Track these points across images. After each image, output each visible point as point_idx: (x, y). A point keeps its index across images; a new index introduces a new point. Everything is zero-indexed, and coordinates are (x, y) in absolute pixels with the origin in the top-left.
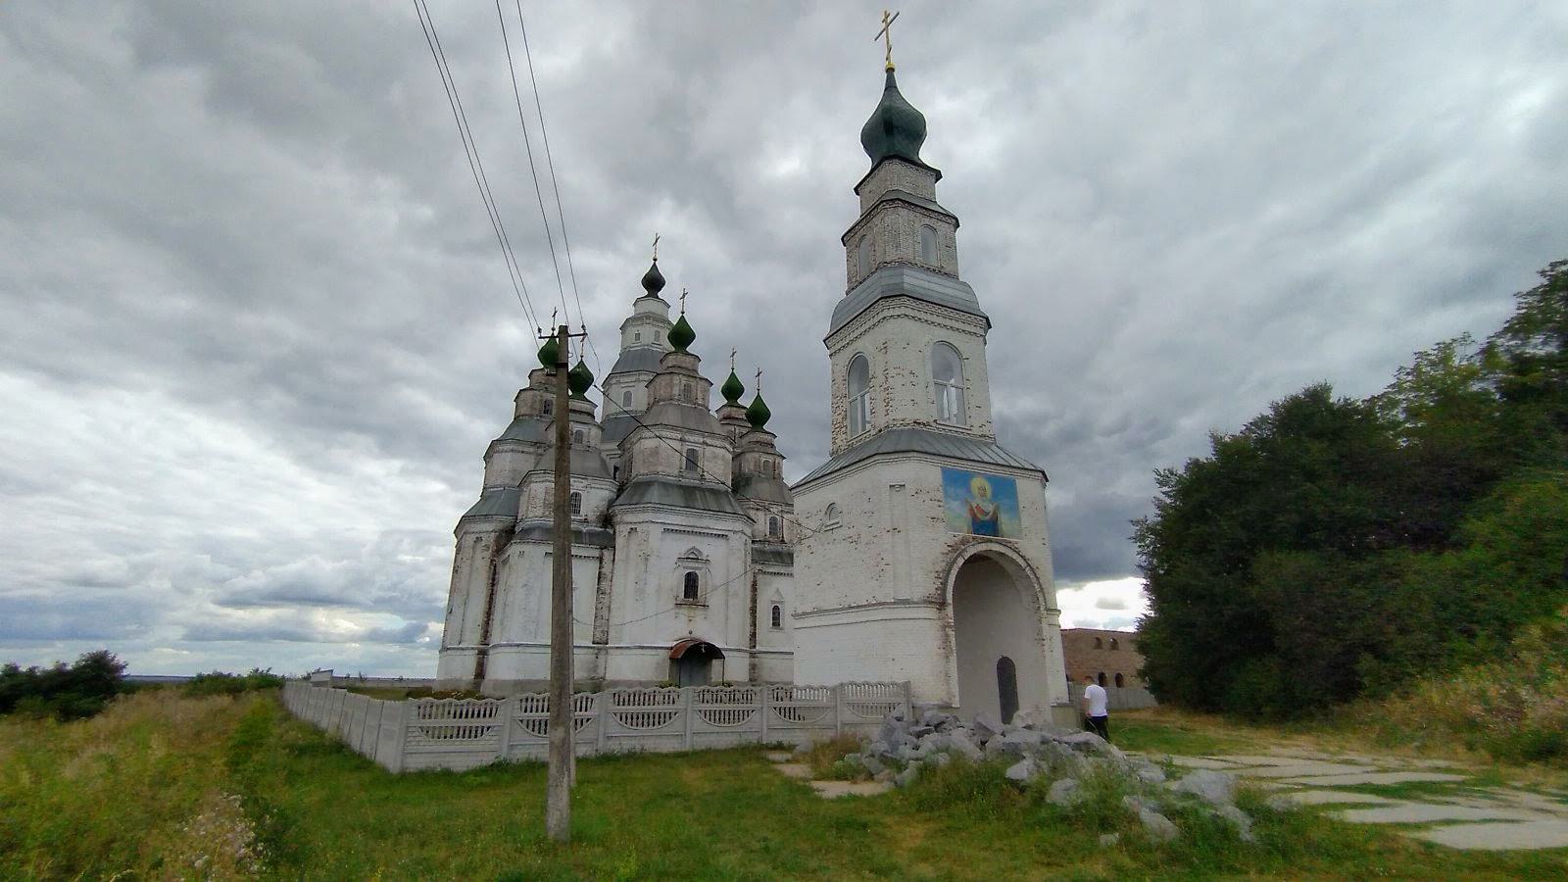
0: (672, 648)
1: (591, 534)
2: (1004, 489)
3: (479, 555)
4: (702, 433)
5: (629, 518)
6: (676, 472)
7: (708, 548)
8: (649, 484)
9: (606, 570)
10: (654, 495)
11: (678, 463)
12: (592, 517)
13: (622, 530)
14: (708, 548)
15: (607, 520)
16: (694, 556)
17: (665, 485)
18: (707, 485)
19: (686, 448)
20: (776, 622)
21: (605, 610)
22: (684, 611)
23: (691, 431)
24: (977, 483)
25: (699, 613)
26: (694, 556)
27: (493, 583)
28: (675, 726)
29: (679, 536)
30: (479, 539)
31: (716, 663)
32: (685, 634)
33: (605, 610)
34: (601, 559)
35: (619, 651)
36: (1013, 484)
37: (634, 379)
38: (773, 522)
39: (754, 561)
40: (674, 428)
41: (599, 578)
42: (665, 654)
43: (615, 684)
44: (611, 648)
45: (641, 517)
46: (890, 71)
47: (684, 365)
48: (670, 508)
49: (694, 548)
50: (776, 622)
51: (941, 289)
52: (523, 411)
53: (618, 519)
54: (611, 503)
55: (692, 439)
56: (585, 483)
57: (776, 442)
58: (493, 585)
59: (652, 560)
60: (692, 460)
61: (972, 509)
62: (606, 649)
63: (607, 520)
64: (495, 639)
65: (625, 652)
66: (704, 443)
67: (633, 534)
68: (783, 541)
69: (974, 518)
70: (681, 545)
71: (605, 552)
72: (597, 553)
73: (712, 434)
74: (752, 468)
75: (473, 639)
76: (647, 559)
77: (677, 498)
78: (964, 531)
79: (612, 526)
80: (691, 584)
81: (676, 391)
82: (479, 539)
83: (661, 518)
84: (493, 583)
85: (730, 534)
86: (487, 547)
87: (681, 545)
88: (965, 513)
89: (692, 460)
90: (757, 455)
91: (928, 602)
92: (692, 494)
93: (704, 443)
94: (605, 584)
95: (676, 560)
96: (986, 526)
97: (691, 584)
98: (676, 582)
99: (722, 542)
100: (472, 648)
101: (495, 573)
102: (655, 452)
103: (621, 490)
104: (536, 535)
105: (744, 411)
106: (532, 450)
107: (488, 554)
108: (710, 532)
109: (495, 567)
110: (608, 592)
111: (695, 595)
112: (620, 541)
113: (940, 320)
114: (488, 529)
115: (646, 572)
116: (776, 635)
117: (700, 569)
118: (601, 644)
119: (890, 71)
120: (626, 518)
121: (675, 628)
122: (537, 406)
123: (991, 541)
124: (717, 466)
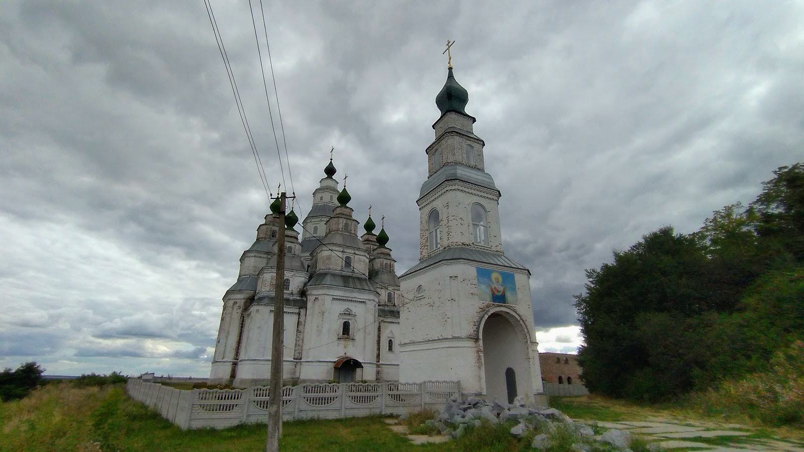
0: (335, 362)
1: (294, 301)
2: (508, 279)
3: (235, 311)
4: (354, 248)
5: (315, 292)
6: (339, 268)
7: (356, 308)
8: (325, 274)
9: (302, 319)
10: (328, 280)
11: (341, 264)
12: (295, 292)
13: (311, 299)
14: (356, 308)
15: (303, 293)
16: (348, 313)
17: (334, 275)
18: (355, 275)
19: (345, 256)
20: (390, 349)
21: (301, 341)
22: (342, 342)
23: (348, 247)
24: (494, 275)
25: (350, 343)
26: (348, 313)
27: (242, 326)
28: (336, 404)
29: (340, 302)
30: (236, 303)
31: (358, 370)
32: (342, 354)
33: (301, 341)
34: (299, 314)
35: (308, 363)
36: (513, 276)
37: (319, 220)
38: (389, 295)
39: (379, 316)
40: (339, 245)
41: (298, 324)
42: (332, 365)
43: (304, 381)
44: (303, 362)
45: (321, 292)
46: (450, 69)
47: (345, 213)
48: (337, 287)
49: (348, 308)
50: (390, 349)
51: (475, 177)
52: (261, 236)
53: (309, 292)
54: (305, 284)
55: (348, 251)
56: (292, 273)
57: (391, 253)
58: (242, 327)
59: (326, 315)
60: (348, 262)
61: (492, 290)
62: (301, 362)
63: (303, 293)
64: (242, 356)
65: (310, 363)
66: (355, 253)
67: (316, 302)
68: (394, 305)
69: (493, 294)
70: (341, 307)
71: (302, 310)
72: (297, 311)
73: (359, 249)
74: (379, 266)
75: (230, 356)
76: (323, 314)
77: (340, 282)
78: (488, 300)
79: (306, 296)
80: (346, 327)
81: (341, 226)
82: (236, 303)
83: (332, 292)
84: (242, 326)
85: (367, 301)
86: (240, 307)
87: (341, 307)
88: (489, 292)
89: (348, 262)
90: (381, 260)
91: (469, 338)
92: (348, 280)
93: (355, 253)
94: (301, 327)
95: (338, 314)
96: (499, 298)
97: (346, 327)
98: (338, 327)
99: (362, 305)
100: (230, 362)
101: (243, 321)
102: (329, 258)
103: (310, 278)
104: (266, 301)
105: (376, 237)
106: (265, 256)
107: (240, 311)
108: (357, 300)
109: (243, 317)
110: (302, 331)
111: (348, 334)
112: (309, 305)
113: (476, 192)
114: (240, 298)
115: (323, 321)
116: (390, 355)
117: (349, 319)
118: (298, 360)
119: (450, 69)
120: (313, 292)
121: (337, 351)
122: (269, 233)
123: (502, 306)
124: (361, 265)
